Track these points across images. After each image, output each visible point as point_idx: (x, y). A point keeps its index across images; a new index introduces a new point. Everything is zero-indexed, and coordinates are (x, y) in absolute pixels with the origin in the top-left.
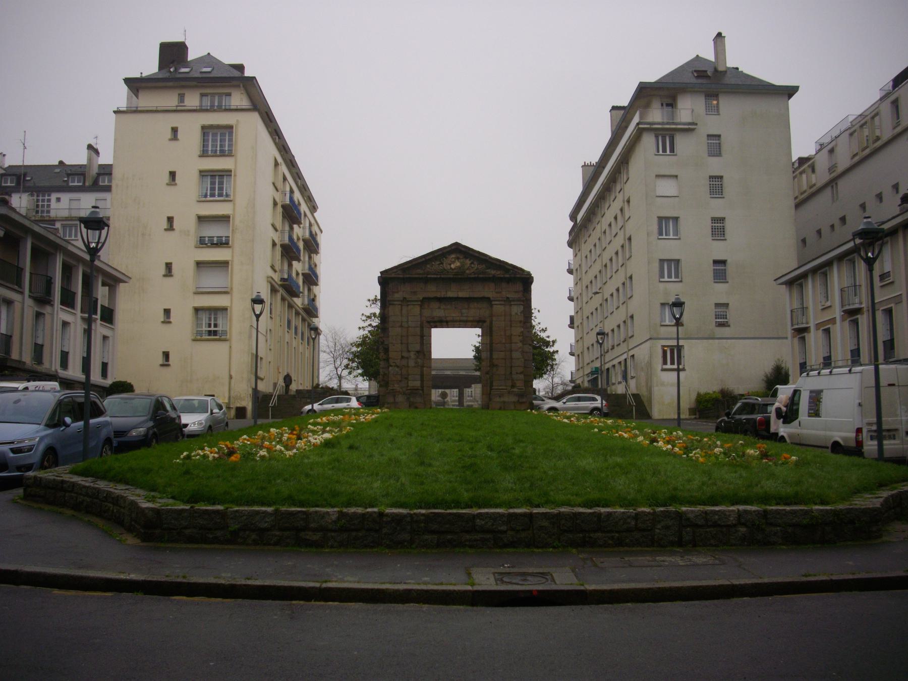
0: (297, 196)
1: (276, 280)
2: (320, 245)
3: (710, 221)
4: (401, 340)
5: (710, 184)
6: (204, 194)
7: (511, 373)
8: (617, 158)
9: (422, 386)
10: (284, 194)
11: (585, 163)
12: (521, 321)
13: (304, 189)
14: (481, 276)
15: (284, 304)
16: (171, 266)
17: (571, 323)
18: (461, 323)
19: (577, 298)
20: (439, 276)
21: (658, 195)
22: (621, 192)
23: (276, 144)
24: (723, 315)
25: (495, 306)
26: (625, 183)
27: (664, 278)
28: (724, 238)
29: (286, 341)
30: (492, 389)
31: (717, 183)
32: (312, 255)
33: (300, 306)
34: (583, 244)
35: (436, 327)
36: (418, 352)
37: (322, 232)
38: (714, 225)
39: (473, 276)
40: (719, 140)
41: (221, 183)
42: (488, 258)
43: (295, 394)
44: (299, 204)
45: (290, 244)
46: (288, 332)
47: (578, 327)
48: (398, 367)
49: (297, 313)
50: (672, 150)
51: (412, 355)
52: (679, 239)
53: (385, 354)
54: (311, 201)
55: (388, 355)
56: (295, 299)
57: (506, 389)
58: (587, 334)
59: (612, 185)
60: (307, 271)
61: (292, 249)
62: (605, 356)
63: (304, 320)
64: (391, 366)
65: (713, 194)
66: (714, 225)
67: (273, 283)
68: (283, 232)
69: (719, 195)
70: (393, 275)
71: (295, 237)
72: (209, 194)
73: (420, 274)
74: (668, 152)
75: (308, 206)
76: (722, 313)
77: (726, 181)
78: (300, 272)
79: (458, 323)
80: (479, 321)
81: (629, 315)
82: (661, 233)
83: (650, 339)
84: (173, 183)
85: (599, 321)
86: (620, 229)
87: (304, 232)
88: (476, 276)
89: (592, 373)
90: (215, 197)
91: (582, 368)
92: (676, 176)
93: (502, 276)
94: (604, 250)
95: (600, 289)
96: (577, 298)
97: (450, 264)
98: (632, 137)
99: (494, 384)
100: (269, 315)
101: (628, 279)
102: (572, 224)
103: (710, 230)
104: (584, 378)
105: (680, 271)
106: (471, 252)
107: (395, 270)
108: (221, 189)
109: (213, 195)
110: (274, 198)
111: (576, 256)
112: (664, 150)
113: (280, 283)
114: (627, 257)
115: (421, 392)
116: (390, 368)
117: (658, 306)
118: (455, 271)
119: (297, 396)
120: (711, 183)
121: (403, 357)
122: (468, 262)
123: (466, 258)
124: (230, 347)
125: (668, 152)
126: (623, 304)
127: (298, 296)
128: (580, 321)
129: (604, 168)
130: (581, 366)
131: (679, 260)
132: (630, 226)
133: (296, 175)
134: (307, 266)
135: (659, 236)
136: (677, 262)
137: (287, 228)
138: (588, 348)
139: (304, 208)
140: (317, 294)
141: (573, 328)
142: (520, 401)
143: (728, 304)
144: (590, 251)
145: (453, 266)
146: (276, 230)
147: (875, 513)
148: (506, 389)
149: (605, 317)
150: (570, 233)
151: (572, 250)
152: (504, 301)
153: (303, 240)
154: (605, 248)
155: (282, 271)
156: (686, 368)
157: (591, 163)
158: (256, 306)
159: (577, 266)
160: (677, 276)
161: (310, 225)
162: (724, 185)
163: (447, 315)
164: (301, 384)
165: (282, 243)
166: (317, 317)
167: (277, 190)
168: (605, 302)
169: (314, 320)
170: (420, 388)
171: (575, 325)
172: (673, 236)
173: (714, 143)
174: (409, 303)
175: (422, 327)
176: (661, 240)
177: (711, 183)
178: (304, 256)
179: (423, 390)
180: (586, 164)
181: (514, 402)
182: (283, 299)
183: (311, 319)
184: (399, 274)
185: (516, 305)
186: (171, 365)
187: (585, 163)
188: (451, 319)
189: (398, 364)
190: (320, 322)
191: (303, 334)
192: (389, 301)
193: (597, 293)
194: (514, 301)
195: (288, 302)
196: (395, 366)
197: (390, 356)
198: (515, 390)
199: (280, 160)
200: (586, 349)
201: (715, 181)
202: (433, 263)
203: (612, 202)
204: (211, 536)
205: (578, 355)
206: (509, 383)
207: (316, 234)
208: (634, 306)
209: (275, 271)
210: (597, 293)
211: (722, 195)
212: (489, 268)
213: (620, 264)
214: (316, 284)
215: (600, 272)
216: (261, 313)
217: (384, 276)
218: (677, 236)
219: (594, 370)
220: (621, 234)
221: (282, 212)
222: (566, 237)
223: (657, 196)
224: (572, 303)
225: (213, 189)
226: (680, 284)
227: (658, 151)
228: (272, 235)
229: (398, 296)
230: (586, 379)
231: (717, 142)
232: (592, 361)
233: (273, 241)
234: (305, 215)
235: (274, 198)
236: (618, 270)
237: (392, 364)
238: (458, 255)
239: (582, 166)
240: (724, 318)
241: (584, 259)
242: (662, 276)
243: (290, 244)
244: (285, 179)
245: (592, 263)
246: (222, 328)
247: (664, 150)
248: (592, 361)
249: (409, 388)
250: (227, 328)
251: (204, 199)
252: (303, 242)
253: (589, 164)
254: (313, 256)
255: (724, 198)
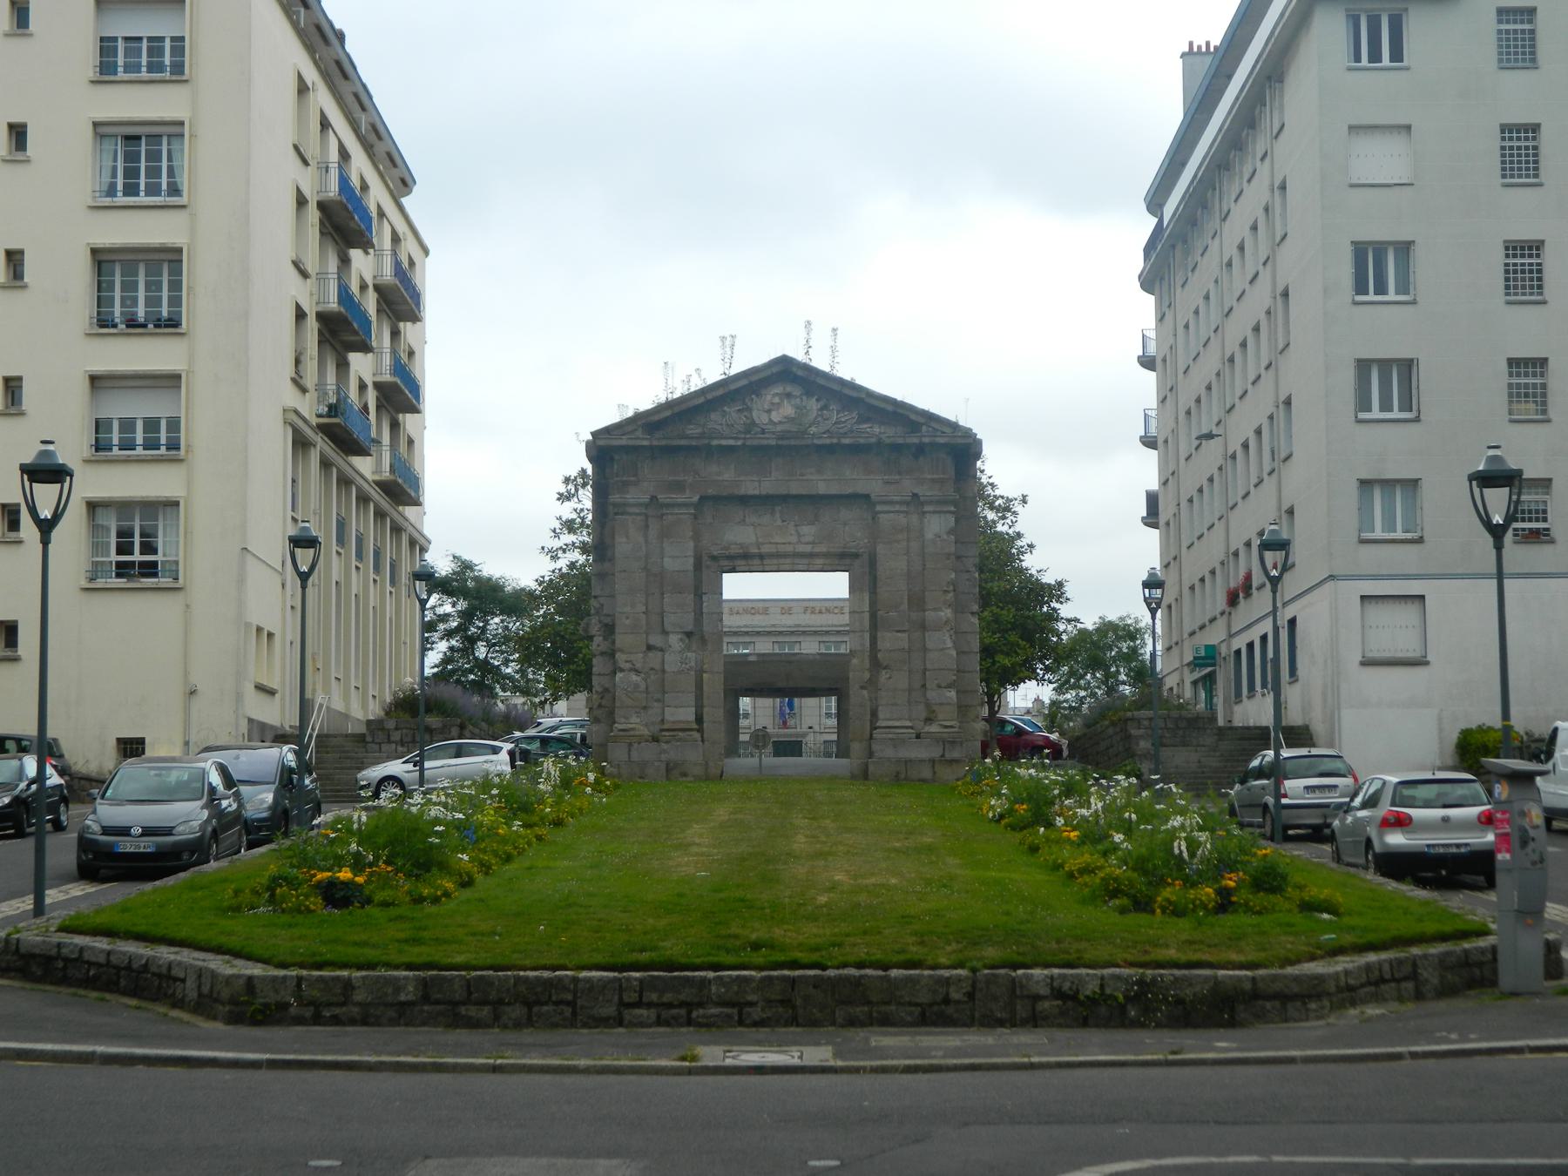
0: (360, 163)
1: (307, 416)
2: (422, 297)
3: (1502, 252)
4: (646, 605)
5: (1503, 148)
6: (105, 188)
7: (924, 686)
8: (1254, 67)
9: (699, 719)
10: (324, 170)
11: (1191, 44)
12: (949, 554)
13: (374, 137)
14: (846, 441)
15: (328, 476)
16: (21, 387)
17: (1149, 513)
18: (797, 561)
19: (1166, 441)
20: (739, 443)
21: (1355, 181)
22: (1267, 160)
23: (295, 25)
24: (1537, 512)
25: (881, 516)
26: (1276, 137)
27: (1369, 410)
28: (1539, 298)
29: (335, 578)
30: (876, 728)
31: (1523, 144)
32: (401, 325)
33: (370, 477)
34: (1179, 290)
35: (733, 570)
36: (689, 635)
37: (426, 252)
38: (1512, 261)
39: (828, 441)
40: (1530, 22)
41: (154, 156)
42: (864, 396)
43: (362, 729)
44: (365, 187)
45: (342, 310)
46: (338, 553)
47: (1168, 524)
48: (637, 672)
49: (363, 499)
50: (1397, 55)
51: (674, 640)
52: (1414, 302)
53: (605, 639)
54: (395, 165)
55: (613, 642)
56: (357, 461)
57: (912, 728)
58: (1189, 547)
59: (1248, 135)
60: (387, 377)
61: (350, 324)
62: (1230, 614)
63: (380, 515)
64: (622, 670)
65: (1512, 176)
66: (1512, 261)
67: (300, 423)
68: (322, 276)
69: (1528, 176)
70: (624, 442)
71: (354, 287)
72: (120, 187)
73: (672, 514)
74: (1386, 61)
75: (387, 186)
76: (1533, 507)
77: (1546, 138)
78: (369, 381)
79: (788, 561)
80: (842, 556)
81: (1285, 507)
82: (1361, 288)
83: (1332, 577)
84: (19, 155)
85: (1218, 517)
86: (1265, 264)
87: (379, 265)
88: (835, 441)
89: (1196, 663)
90: (138, 195)
91: (1177, 644)
92: (1408, 128)
93: (900, 441)
94: (1227, 315)
95: (1218, 423)
96: (1166, 441)
97: (769, 411)
98: (1287, 14)
99: (881, 715)
100: (290, 513)
101: (1281, 406)
102: (1152, 222)
103: (1502, 276)
104: (1182, 674)
105: (1414, 392)
106: (821, 381)
107: (630, 428)
108: (154, 172)
109: (131, 190)
110: (298, 188)
111: (1161, 318)
112: (1375, 56)
113: (314, 421)
114: (1281, 346)
115: (697, 735)
116: (619, 675)
117: (1353, 490)
118: (779, 428)
119: (369, 739)
120: (1507, 144)
121: (650, 648)
122: (813, 405)
123: (809, 394)
124: (188, 606)
125: (1386, 61)
126: (1270, 474)
127: (362, 451)
128: (1172, 509)
129: (1230, 77)
130: (1174, 640)
131: (1412, 360)
132: (1287, 254)
133: (350, 99)
134: (387, 360)
135: (1358, 293)
136: (1407, 367)
137: (333, 264)
138: (1192, 588)
139: (378, 195)
140: (414, 436)
141: (1154, 526)
142: (948, 756)
143: (1550, 480)
144: (1197, 312)
145: (775, 417)
146: (304, 274)
147: (1316, 982)
148: (912, 728)
149: (1230, 505)
150: (1149, 249)
151: (1153, 297)
152: (908, 504)
153: (377, 288)
154: (1231, 309)
155: (321, 386)
156: (1429, 658)
157: (1208, 44)
158: (298, 551)
159: (1166, 349)
160: (1406, 405)
161: (396, 239)
162: (1544, 151)
163: (760, 540)
164: (374, 697)
165: (320, 308)
166: (416, 502)
167: (305, 163)
168: (1229, 461)
169: (409, 511)
170: (695, 726)
171: (1162, 520)
172: (1397, 293)
173: (1515, 31)
174: (665, 511)
175: (698, 566)
176: (1360, 306)
177: (1507, 144)
178: (381, 337)
179: (701, 730)
180: (1195, 49)
181: (933, 761)
182: (326, 464)
183: (401, 508)
184: (638, 438)
185: (934, 512)
186: (22, 657)
187: (1191, 44)
188: (773, 549)
189: (638, 666)
190: (425, 513)
191: (377, 554)
192: (615, 505)
193: (1210, 436)
194: (931, 503)
195: (339, 471)
196: (631, 670)
197: (618, 644)
198: (934, 728)
199: (312, 75)
200: (1186, 591)
201: (1519, 139)
202: (725, 408)
203: (1245, 184)
204: (328, 1015)
205: (1170, 607)
206: (921, 712)
207: (412, 263)
208: (1299, 480)
209: (304, 390)
210: (1210, 436)
211: (1536, 176)
212: (868, 420)
213: (1264, 363)
214: (415, 410)
215: (1218, 374)
216: (312, 568)
217: (601, 443)
218: (1406, 292)
219: (1203, 654)
220: (1265, 276)
221: (320, 220)
222: (1138, 263)
223: (1352, 186)
224: (1153, 454)
225: (131, 173)
226: (1413, 427)
227: (1358, 59)
228: (294, 293)
229: (637, 495)
230: (1189, 678)
231: (1527, 27)
232: (1202, 627)
233: (299, 308)
234: (381, 214)
235: (298, 188)
236: (1259, 377)
237: (623, 665)
238: (789, 389)
239: (1183, 55)
240: (1537, 520)
241: (1181, 330)
242: (1363, 403)
243: (342, 310)
244: (325, 124)
245: (1191, 362)
246: (164, 555)
247: (1375, 56)
248: (1202, 627)
249: (665, 727)
250: (177, 555)
251: (107, 201)
252: (376, 295)
253: (1204, 49)
254: (407, 328)
255: (1540, 185)
